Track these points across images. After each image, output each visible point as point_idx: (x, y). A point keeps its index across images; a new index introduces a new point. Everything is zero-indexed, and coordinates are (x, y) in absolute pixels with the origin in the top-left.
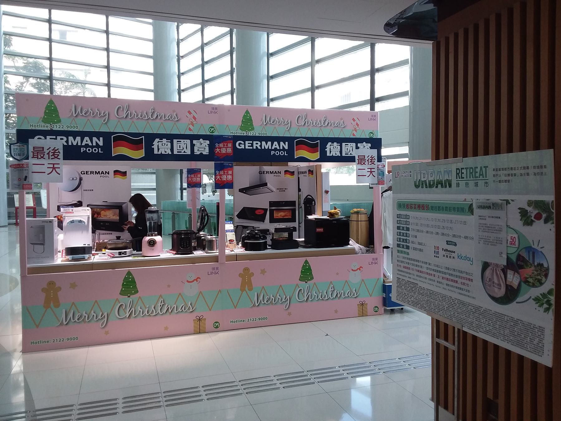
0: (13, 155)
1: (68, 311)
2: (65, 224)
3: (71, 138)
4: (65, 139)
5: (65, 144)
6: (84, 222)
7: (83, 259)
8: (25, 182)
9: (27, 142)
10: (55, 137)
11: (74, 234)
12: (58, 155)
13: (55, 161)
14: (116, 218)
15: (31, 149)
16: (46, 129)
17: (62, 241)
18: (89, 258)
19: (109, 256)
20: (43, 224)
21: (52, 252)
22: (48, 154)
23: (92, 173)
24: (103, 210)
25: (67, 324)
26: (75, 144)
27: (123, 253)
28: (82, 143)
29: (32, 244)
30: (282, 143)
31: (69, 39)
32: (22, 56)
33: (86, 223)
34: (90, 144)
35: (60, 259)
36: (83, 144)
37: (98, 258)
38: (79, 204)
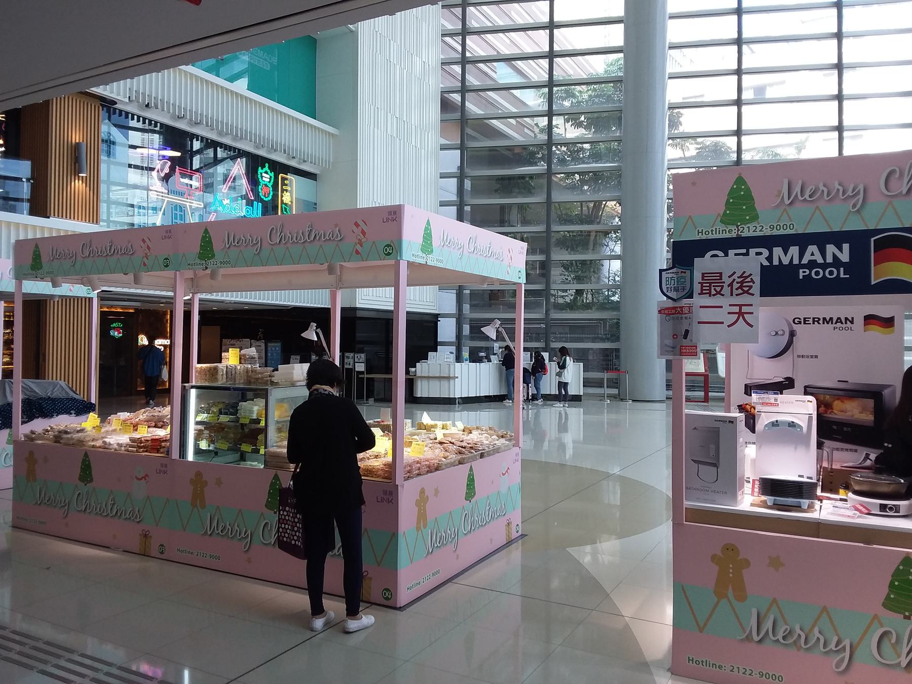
0: (665, 291)
1: (763, 613)
2: (759, 426)
3: (778, 251)
4: (766, 253)
5: (766, 263)
6: (800, 427)
7: (798, 508)
8: (685, 342)
9: (690, 265)
10: (744, 251)
11: (778, 451)
12: (751, 287)
13: (744, 299)
14: (868, 418)
15: (697, 277)
16: (728, 235)
17: (754, 461)
18: (811, 507)
19: (857, 509)
20: (718, 424)
21: (732, 486)
22: (731, 285)
23: (816, 320)
24: (839, 398)
25: (760, 641)
26: (786, 261)
27: (891, 509)
28: (801, 256)
29: (695, 461)
31: (770, 94)
32: (693, 137)
33: (805, 429)
34: (820, 260)
35: (748, 501)
36: (805, 261)
37: (830, 509)
38: (784, 385)
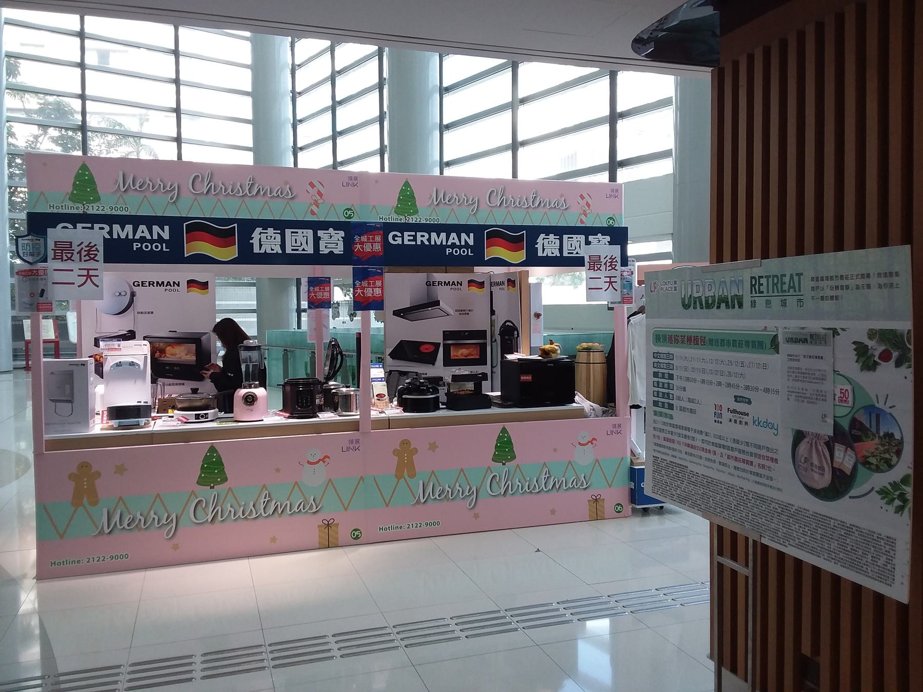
0: (21, 255)
1: (112, 511)
2: (106, 368)
3: (116, 227)
4: (107, 228)
5: (108, 237)
6: (138, 365)
7: (137, 426)
8: (41, 300)
9: (44, 234)
10: (90, 225)
11: (121, 384)
12: (96, 255)
13: (91, 265)
14: (192, 358)
15: (51, 245)
16: (75, 211)
17: (102, 396)
18: (147, 424)
19: (179, 420)
20: (72, 368)
21: (85, 415)
22: (80, 252)
23: (151, 284)
24: (170, 344)
25: (109, 533)
26: (123, 236)
27: (202, 416)
28: (134, 234)
29: (52, 401)
30: (463, 236)
31: (113, 64)
32: (35, 92)
33: (142, 367)
34: (149, 237)
35: (98, 426)
36: (137, 237)
37: (161, 424)
38: (130, 336)
